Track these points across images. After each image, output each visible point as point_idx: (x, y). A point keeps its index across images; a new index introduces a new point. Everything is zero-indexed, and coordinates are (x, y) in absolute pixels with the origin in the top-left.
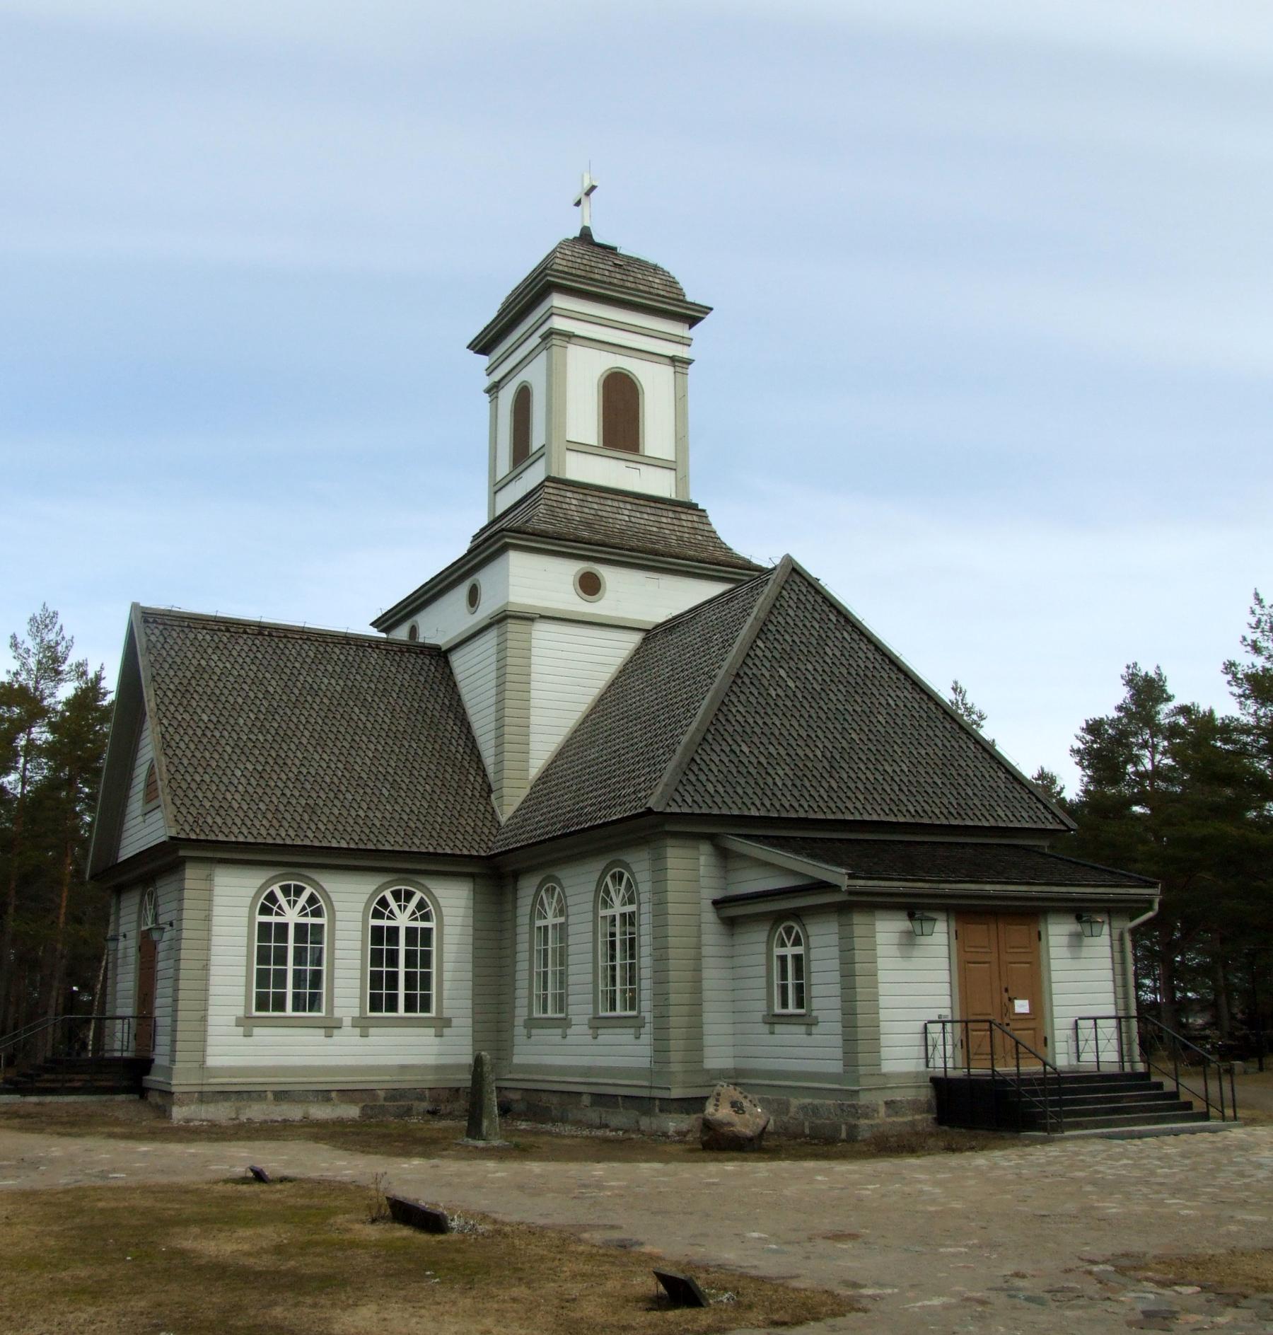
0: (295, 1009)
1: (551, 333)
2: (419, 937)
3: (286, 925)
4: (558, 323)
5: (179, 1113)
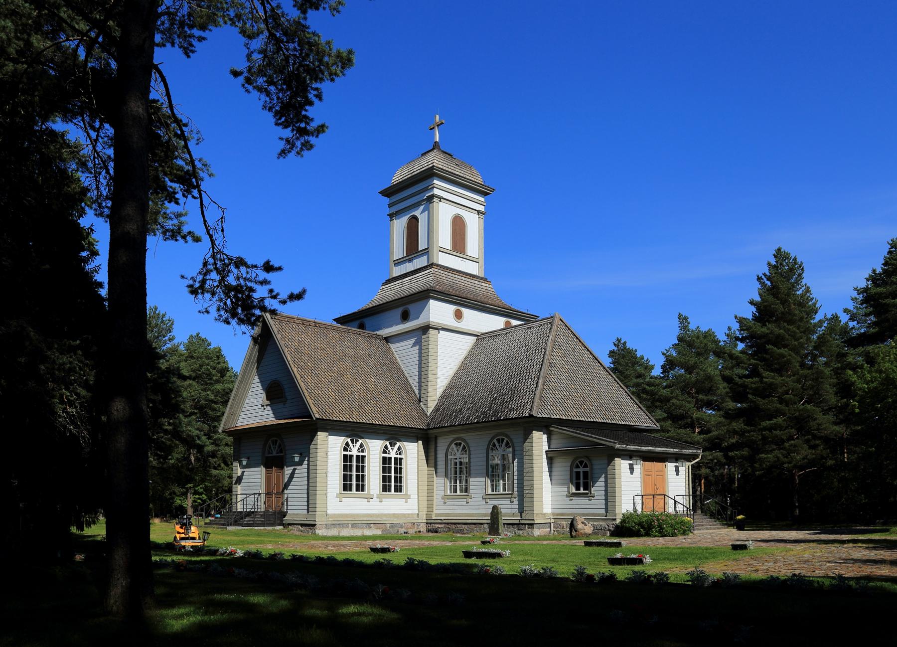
1: (433, 196)
2: (399, 461)
4: (436, 192)
5: (320, 532)
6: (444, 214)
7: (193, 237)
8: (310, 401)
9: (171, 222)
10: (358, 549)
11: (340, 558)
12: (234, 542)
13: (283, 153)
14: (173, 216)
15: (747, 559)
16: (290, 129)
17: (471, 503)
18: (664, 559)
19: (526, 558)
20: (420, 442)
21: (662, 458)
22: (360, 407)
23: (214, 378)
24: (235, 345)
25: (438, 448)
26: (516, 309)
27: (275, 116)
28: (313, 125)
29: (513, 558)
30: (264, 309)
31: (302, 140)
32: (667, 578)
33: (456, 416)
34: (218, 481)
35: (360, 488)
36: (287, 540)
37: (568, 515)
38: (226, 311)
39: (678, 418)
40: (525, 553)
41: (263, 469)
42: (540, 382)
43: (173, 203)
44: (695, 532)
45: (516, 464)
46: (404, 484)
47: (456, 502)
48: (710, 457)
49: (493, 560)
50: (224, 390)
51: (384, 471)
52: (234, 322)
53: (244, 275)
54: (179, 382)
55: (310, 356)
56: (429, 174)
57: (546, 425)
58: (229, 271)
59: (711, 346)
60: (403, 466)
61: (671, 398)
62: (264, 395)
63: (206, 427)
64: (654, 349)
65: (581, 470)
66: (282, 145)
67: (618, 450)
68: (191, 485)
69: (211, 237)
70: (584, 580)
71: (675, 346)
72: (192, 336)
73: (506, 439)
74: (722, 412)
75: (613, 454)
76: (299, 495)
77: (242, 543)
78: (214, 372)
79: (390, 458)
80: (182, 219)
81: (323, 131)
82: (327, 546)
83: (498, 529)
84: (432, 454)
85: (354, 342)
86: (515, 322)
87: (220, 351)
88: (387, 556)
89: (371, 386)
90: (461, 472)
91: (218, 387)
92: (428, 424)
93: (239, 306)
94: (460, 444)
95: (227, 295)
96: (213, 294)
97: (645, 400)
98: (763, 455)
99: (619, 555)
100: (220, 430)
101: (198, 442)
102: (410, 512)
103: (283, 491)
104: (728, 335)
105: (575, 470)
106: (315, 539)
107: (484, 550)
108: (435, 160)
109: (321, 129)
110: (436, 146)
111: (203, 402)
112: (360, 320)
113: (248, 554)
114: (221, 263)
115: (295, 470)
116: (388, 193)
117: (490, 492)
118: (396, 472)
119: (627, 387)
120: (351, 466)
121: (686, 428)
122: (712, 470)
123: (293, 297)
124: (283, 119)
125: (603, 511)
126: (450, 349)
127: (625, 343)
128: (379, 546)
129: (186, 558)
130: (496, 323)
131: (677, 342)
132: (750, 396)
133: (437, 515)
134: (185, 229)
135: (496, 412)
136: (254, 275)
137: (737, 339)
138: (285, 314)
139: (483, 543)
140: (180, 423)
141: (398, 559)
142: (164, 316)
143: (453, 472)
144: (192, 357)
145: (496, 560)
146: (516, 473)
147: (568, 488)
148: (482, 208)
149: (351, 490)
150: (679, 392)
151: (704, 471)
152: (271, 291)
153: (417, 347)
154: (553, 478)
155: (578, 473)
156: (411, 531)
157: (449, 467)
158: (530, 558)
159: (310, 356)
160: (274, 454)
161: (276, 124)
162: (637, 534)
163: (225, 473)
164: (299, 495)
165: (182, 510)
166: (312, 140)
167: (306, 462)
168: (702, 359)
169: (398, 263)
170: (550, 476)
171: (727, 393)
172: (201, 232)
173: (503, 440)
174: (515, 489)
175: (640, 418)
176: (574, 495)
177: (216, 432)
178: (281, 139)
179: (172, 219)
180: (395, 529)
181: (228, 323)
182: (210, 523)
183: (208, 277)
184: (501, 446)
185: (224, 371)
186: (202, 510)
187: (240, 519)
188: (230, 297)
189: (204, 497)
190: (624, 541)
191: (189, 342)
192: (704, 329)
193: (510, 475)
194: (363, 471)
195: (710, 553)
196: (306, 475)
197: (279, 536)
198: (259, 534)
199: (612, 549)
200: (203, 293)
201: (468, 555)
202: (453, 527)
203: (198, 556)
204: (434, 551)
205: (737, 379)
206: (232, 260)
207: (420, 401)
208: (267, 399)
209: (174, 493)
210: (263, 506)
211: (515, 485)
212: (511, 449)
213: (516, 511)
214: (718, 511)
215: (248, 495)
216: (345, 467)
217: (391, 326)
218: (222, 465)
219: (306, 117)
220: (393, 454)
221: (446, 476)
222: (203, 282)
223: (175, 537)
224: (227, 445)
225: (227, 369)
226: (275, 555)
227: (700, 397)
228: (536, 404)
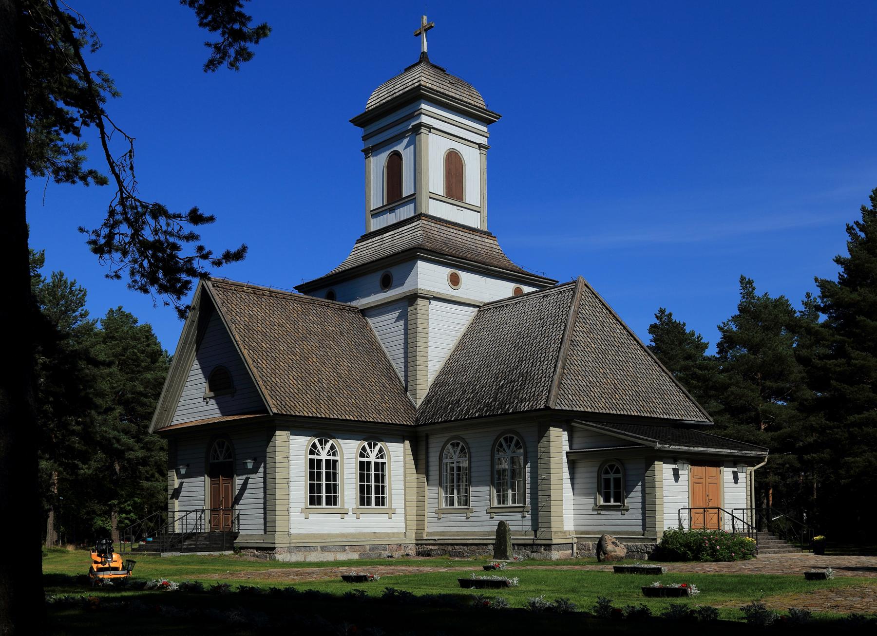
0: (327, 504)
1: (420, 125)
2: (380, 467)
3: (321, 460)
4: (424, 119)
5: (280, 557)
6: (435, 149)
7: (96, 177)
8: (266, 392)
9: (64, 158)
10: (327, 578)
11: (302, 589)
12: (167, 571)
13: (211, 65)
14: (66, 149)
15: (825, 591)
16: (220, 31)
17: (471, 519)
18: (716, 590)
19: (539, 587)
20: (407, 442)
21: (717, 462)
22: (330, 398)
23: (143, 364)
24: (165, 322)
25: (431, 450)
26: (529, 272)
27: (198, 14)
28: (252, 26)
29: (521, 587)
30: (192, 272)
31: (237, 46)
32: (716, 614)
33: (452, 409)
34: (152, 495)
35: (332, 500)
36: (238, 568)
37: (594, 533)
38: (143, 275)
39: (738, 411)
40: (538, 581)
41: (208, 479)
42: (560, 365)
43: (70, 134)
44: (759, 556)
45: (528, 470)
46: (387, 495)
47: (452, 517)
48: (780, 461)
49: (496, 591)
50: (155, 380)
51: (362, 480)
52: (153, 289)
53: (164, 228)
54: (89, 370)
55: (264, 334)
56: (416, 95)
57: (566, 419)
58: (144, 223)
59: (783, 318)
60: (386, 473)
61: (729, 385)
62: (206, 385)
63: (133, 428)
64: (708, 323)
65: (612, 476)
66: (209, 53)
67: (659, 450)
68: (115, 502)
69: (117, 177)
70: (607, 616)
71: (735, 319)
72: (111, 311)
73: (516, 438)
74: (796, 403)
75: (653, 457)
76: (254, 511)
77: (180, 573)
78: (142, 357)
79: (369, 463)
80: (80, 154)
81: (265, 35)
82: (288, 574)
83: (505, 551)
84: (422, 457)
85: (322, 317)
86: (527, 289)
87: (149, 330)
88: (361, 586)
89: (344, 373)
90: (459, 480)
91: (149, 376)
92: (417, 420)
93: (159, 268)
94: (458, 444)
95: (142, 254)
96: (125, 253)
97: (695, 387)
98: (850, 459)
99: (657, 585)
100: (151, 431)
101: (116, 445)
102: (395, 530)
103: (233, 506)
104: (806, 304)
105: (604, 476)
106: (274, 566)
107: (485, 577)
108: (423, 77)
109: (262, 31)
110: (423, 58)
111: (129, 395)
112: (330, 288)
113: (184, 587)
114: (131, 212)
115: (247, 479)
116: (363, 121)
117: (496, 504)
118: (377, 481)
119: (672, 371)
120: (319, 474)
121: (748, 423)
122: (784, 478)
123: (229, 257)
124: (210, 18)
125: (640, 529)
126: (446, 322)
127: (670, 314)
128: (354, 574)
129: (103, 594)
130: (503, 290)
131: (738, 313)
132: (833, 382)
133: (429, 534)
134: (84, 168)
135: (502, 404)
136: (176, 228)
137: (818, 308)
138: (230, 281)
139: (487, 568)
140: (92, 422)
141: (374, 590)
142: (73, 284)
143: (449, 480)
144: (113, 338)
145: (501, 590)
146: (528, 481)
147: (595, 499)
148: (484, 141)
149: (319, 503)
150: (739, 377)
151: (772, 478)
152: (201, 249)
153: (402, 322)
154: (576, 486)
155: (607, 481)
156: (396, 555)
157: (444, 473)
158: (544, 587)
159: (264, 334)
160: (221, 459)
161: (201, 24)
162: (683, 558)
163: (159, 485)
164: (254, 511)
165: (106, 534)
166: (250, 46)
167: (261, 469)
168: (771, 335)
169: (377, 213)
170: (572, 484)
171: (803, 378)
172: (104, 170)
173: (512, 438)
174: (528, 501)
175: (690, 412)
176: (603, 508)
177: (146, 433)
178: (208, 45)
179: (65, 154)
180: (375, 553)
181: (146, 291)
182: (140, 549)
183: (116, 231)
184: (509, 447)
185: (156, 355)
186: (130, 533)
187: (179, 542)
188: (147, 257)
189: (133, 515)
190: (665, 567)
191: (109, 318)
192: (774, 296)
193: (522, 485)
194: (335, 480)
195: (776, 583)
196: (262, 485)
197: (230, 563)
198: (202, 562)
199: (650, 577)
200: (110, 252)
201: (465, 583)
202: (449, 549)
203: (119, 591)
204: (423, 580)
205: (816, 361)
206: (147, 207)
207: (406, 390)
208: (211, 390)
209: (94, 512)
210: (208, 526)
211: (528, 496)
212: (522, 451)
213: (528, 528)
214: (790, 530)
215: (188, 513)
216: (312, 476)
217: (369, 295)
218: (157, 475)
219: (241, 15)
220: (373, 458)
221: (440, 485)
222: (110, 237)
223: (92, 568)
224: (162, 449)
225: (159, 353)
226: (219, 587)
227: (768, 383)
228: (553, 393)
